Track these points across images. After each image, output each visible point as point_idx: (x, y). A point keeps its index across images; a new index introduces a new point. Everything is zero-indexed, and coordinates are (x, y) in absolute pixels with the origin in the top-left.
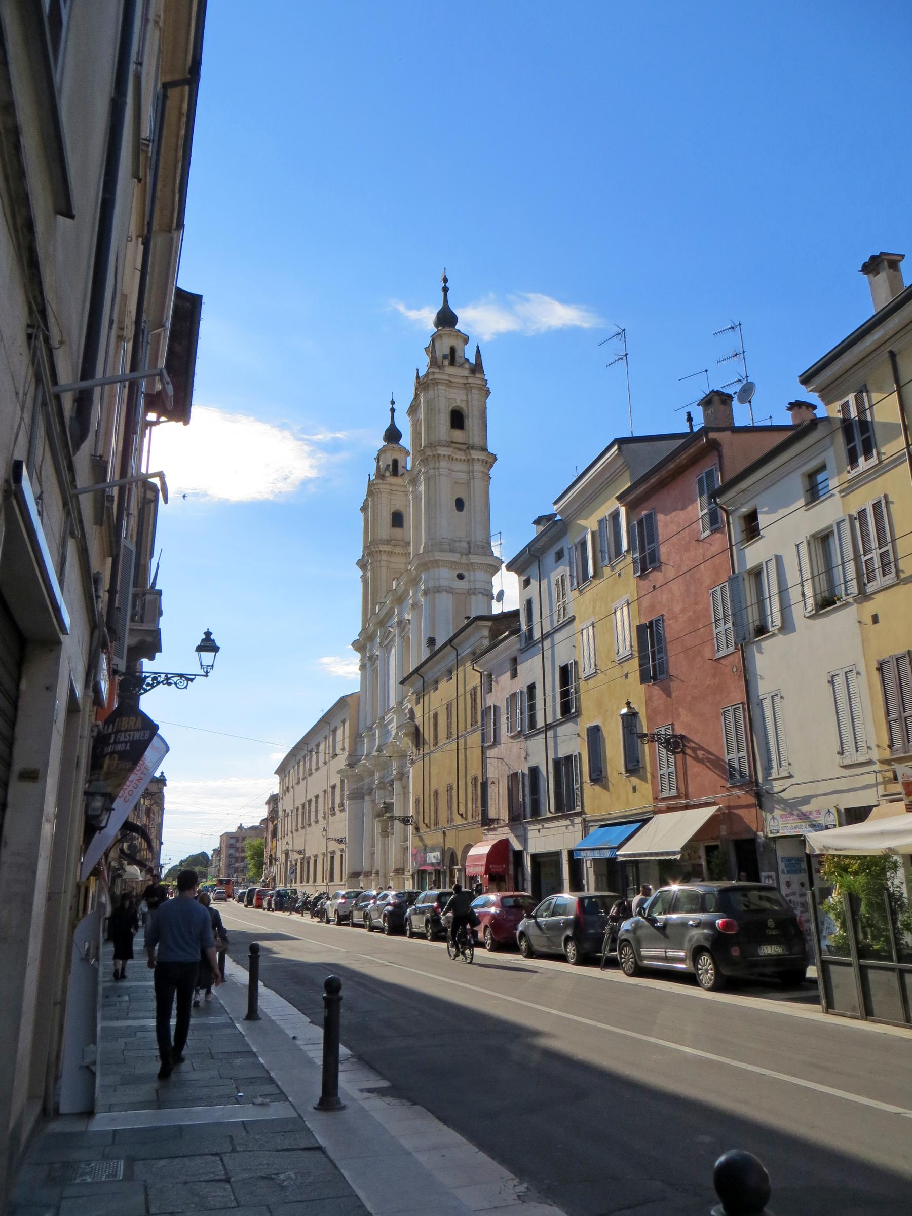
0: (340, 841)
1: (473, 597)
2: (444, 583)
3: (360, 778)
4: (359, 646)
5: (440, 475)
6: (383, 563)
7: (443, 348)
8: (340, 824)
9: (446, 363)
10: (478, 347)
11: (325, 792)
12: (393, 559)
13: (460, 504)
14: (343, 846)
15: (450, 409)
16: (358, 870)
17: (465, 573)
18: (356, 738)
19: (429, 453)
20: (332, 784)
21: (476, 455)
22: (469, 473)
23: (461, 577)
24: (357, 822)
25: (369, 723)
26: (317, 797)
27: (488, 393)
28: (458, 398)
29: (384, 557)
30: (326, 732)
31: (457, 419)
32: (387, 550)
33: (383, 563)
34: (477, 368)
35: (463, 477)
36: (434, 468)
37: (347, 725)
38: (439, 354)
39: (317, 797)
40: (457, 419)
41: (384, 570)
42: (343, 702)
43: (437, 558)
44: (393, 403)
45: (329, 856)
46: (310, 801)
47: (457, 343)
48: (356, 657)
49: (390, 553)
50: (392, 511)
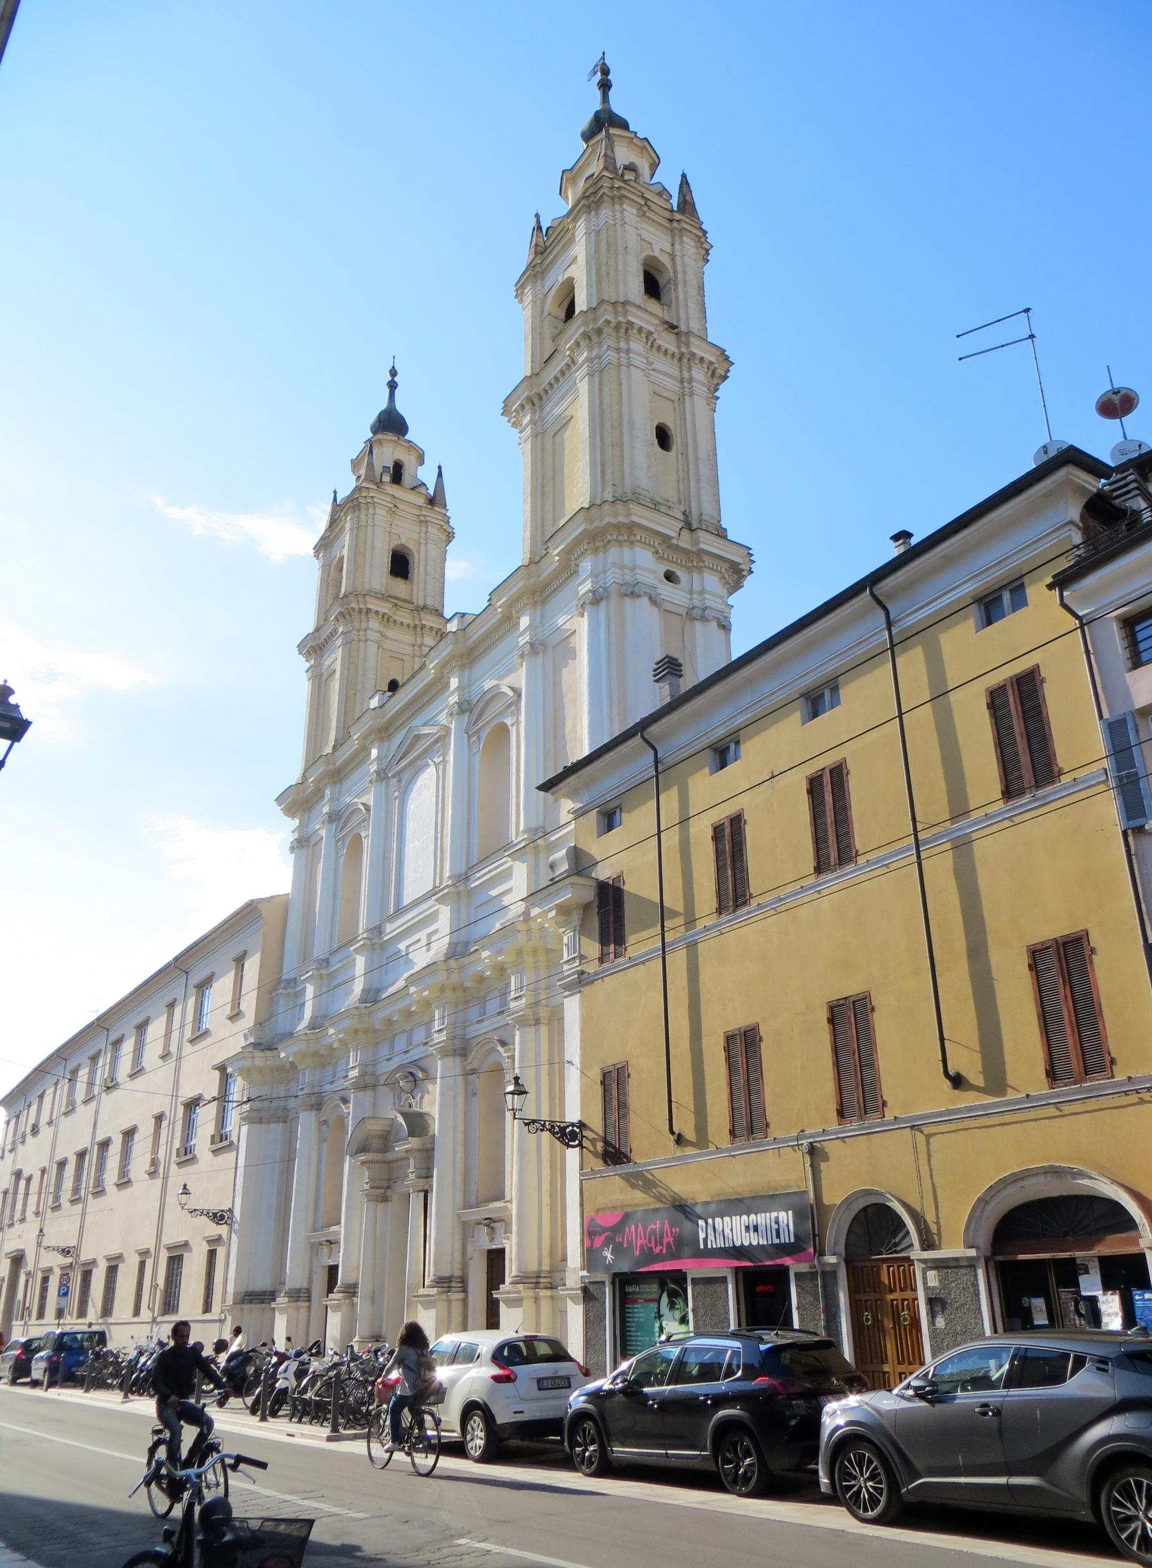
0: (218, 1217)
1: (698, 625)
2: (644, 577)
3: (288, 1071)
4: (297, 802)
5: (629, 365)
6: (372, 635)
7: (386, 455)
8: (219, 1180)
9: (387, 478)
10: (440, 468)
11: (43, 1171)
12: (390, 633)
13: (663, 437)
14: (223, 1230)
15: (643, 255)
16: (262, 1283)
17: (681, 573)
18: (279, 989)
19: (354, 605)
20: (59, 1157)
21: (429, 620)
22: (682, 381)
23: (670, 577)
24: (275, 1173)
25: (320, 950)
26: (129, 1134)
27: (450, 536)
28: (407, 535)
29: (374, 624)
30: (101, 1042)
31: (400, 565)
32: (382, 610)
33: (372, 635)
34: (436, 500)
35: (672, 385)
36: (618, 350)
37: (252, 966)
38: (378, 469)
39: (129, 1134)
40: (400, 565)
41: (372, 647)
42: (248, 916)
43: (634, 519)
44: (393, 373)
45: (40, 1275)
46: (105, 1145)
47: (408, 460)
48: (287, 828)
49: (386, 619)
50: (393, 545)
